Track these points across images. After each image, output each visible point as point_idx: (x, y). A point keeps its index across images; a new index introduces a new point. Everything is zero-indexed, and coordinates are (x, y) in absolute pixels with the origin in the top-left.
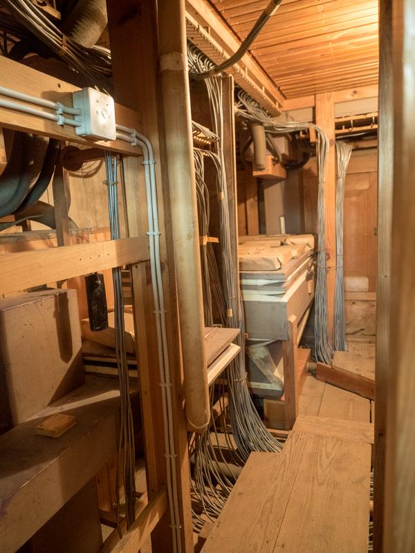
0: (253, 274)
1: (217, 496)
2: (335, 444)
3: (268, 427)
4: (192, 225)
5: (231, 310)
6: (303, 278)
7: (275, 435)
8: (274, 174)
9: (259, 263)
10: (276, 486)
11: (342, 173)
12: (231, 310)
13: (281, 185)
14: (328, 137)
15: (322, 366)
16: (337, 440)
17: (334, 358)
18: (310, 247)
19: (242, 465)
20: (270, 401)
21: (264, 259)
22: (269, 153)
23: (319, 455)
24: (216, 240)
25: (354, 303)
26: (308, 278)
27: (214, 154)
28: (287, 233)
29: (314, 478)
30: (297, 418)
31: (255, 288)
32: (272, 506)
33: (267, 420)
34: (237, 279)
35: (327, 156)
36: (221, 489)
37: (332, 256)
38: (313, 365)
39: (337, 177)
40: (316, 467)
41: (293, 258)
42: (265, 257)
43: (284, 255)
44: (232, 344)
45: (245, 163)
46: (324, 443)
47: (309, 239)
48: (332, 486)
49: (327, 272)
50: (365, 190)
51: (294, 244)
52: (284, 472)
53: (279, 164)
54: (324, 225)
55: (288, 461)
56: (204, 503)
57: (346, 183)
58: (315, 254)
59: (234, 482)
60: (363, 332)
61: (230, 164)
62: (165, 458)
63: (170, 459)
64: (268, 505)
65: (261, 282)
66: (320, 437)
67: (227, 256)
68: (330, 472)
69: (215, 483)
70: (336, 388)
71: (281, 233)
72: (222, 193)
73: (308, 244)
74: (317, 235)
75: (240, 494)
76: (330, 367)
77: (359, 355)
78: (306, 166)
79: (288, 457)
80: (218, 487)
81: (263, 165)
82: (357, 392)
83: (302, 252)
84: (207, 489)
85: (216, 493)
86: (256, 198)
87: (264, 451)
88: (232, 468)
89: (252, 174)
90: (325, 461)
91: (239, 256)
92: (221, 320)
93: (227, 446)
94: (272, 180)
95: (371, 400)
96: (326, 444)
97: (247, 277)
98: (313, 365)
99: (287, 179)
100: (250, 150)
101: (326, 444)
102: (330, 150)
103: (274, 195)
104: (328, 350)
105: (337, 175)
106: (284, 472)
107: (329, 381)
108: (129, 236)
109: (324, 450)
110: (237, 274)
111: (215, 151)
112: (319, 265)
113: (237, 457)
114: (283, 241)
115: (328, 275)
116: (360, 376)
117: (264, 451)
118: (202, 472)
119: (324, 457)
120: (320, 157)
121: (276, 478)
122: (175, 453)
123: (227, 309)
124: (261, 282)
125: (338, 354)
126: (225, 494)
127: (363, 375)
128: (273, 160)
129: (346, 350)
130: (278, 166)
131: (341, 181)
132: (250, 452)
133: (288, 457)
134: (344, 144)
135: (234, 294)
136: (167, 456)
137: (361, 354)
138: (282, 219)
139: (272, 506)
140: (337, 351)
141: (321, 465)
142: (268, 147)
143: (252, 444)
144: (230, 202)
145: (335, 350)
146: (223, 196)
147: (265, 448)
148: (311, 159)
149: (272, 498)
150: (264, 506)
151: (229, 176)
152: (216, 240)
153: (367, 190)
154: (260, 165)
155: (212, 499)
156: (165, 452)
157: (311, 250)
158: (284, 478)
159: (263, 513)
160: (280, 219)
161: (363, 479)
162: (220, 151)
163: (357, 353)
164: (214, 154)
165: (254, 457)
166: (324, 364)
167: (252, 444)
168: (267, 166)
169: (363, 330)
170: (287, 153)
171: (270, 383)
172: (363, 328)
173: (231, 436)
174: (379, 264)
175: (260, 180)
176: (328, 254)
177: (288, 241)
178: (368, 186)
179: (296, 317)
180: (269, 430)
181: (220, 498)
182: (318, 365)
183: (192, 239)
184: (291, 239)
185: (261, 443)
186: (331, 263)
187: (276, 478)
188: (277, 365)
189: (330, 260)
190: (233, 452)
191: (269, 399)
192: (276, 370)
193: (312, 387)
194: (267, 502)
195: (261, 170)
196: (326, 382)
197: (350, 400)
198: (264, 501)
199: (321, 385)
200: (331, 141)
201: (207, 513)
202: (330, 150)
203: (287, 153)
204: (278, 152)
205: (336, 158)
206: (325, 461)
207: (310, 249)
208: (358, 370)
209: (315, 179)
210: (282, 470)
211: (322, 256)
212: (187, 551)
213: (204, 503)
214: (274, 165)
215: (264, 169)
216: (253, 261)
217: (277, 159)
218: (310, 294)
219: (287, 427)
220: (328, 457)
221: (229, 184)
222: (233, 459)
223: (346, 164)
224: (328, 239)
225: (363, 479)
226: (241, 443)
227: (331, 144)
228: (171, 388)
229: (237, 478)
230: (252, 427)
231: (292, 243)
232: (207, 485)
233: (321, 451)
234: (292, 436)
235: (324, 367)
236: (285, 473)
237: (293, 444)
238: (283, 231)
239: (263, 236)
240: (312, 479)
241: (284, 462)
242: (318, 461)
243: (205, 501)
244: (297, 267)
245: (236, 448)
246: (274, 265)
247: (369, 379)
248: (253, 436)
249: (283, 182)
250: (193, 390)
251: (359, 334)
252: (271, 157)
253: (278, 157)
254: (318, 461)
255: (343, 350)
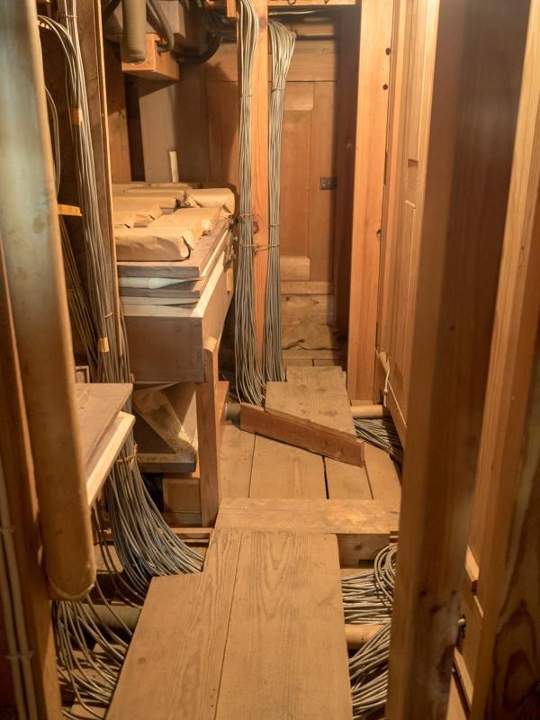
0: (139, 269)
1: (96, 666)
2: (286, 542)
3: (173, 524)
4: (43, 199)
5: (106, 340)
6: (220, 267)
7: (183, 536)
8: (160, 72)
9: (151, 248)
10: (201, 632)
11: (280, 82)
12: (106, 340)
13: (170, 90)
14: (257, 11)
15: (248, 408)
16: (287, 536)
17: (268, 393)
18: (227, 210)
19: (141, 603)
20: (174, 481)
21: (160, 240)
22: (150, 28)
23: (263, 565)
24: (75, 211)
25: (288, 299)
26: (226, 266)
27: (59, 25)
28: (181, 180)
29: (259, 608)
30: (221, 507)
31: (145, 292)
32: (197, 671)
33: (170, 511)
34: (113, 276)
35: (256, 47)
36: (103, 651)
37: (263, 226)
38: (236, 408)
39: (272, 91)
40: (261, 587)
41: (204, 234)
42: (161, 236)
43: (192, 231)
44: (121, 413)
45: (118, 47)
46: (269, 544)
47: (225, 197)
48: (289, 616)
49: (254, 253)
50: (306, 112)
51: (201, 206)
52: (210, 605)
53: (168, 53)
54: (249, 172)
55: (215, 587)
56: (76, 685)
57: (284, 99)
58: (236, 222)
59: (128, 639)
60: (303, 345)
61: (92, 50)
62: (9, 662)
63: (20, 662)
64: (192, 672)
65: (155, 282)
66: (259, 534)
67: (95, 239)
68: (282, 593)
69: (91, 642)
70: (272, 442)
71: (171, 181)
72: (80, 111)
73: (225, 207)
74: (241, 191)
75: (142, 660)
76: (262, 409)
77: (303, 386)
78: (212, 61)
79: (214, 576)
80: (98, 648)
81: (140, 53)
82: (305, 446)
83: (216, 222)
84: (77, 654)
85: (95, 661)
86: (124, 112)
87: (174, 573)
88: (119, 612)
89: (121, 67)
90: (273, 575)
91: (116, 233)
92: (86, 357)
93: (105, 568)
94: (155, 82)
95: (323, 457)
96: (271, 544)
97: (129, 273)
98: (236, 408)
99: (179, 83)
100: (115, 18)
101: (271, 544)
102: (260, 36)
103: (158, 110)
104: (257, 381)
105: (271, 82)
106: (210, 605)
107: (260, 432)
108: (54, 603)
109: (269, 555)
110: (112, 266)
111: (61, 20)
112: (241, 242)
113: (127, 587)
114: (181, 199)
115: (256, 259)
116: (309, 421)
117: (174, 573)
118: (68, 632)
119: (270, 569)
120: (245, 47)
121: (199, 620)
122: (30, 648)
123: (97, 338)
124: (155, 282)
125: (272, 387)
126: (112, 660)
127: (312, 421)
128: (158, 43)
129: (283, 379)
130: (166, 55)
131: (278, 95)
132: (149, 578)
133: (214, 576)
134: (283, 28)
135: (109, 309)
136: (14, 658)
137: (306, 384)
138: (173, 155)
139: (197, 671)
140: (270, 383)
141: (268, 584)
142: (150, 19)
143: (152, 565)
144: (97, 131)
145: (267, 380)
146: (81, 118)
147: (175, 569)
148: (222, 48)
149: (196, 657)
150: (185, 674)
151: (91, 77)
152: (75, 211)
153: (311, 112)
154: (134, 52)
155: (89, 674)
156: (6, 650)
157: (230, 217)
158: (213, 617)
159: (184, 686)
160: (169, 154)
161: (331, 596)
162: (72, 20)
163: (300, 382)
164: (59, 25)
165: (159, 587)
166: (252, 406)
167: (152, 565)
168: (150, 57)
169: (302, 341)
170: (183, 34)
171: (175, 453)
172: (300, 338)
173: (112, 549)
174: (502, 378)
175: (130, 79)
176: (255, 224)
177: (190, 200)
178: (312, 106)
179: (215, 341)
180: (175, 531)
181: (103, 668)
182: (242, 406)
183: (45, 231)
184: (196, 197)
185: (167, 560)
186: (261, 239)
187: (199, 620)
188: (182, 420)
189: (259, 235)
190: (116, 577)
191: (170, 478)
192: (182, 429)
193: (235, 444)
194: (188, 666)
195: (137, 61)
196: (256, 434)
197: (295, 460)
198: (184, 667)
199: (248, 438)
200: (261, 19)
201: (83, 700)
202: (260, 36)
203: (183, 34)
204: (169, 32)
205: (270, 53)
206: (273, 575)
207: (227, 214)
208: (304, 412)
209: (235, 92)
210: (208, 602)
211: (247, 226)
212: (32, 718)
213: (76, 685)
214: (159, 53)
215: (143, 60)
216: (138, 244)
217: (165, 42)
218: (229, 292)
219: (205, 520)
220: (276, 568)
221: (91, 93)
222: (118, 591)
223: (286, 64)
224: (257, 197)
225: (331, 596)
226: (131, 562)
227: (261, 26)
228: (14, 535)
229: (133, 631)
230: (150, 535)
231: (198, 204)
232: (76, 646)
233: (265, 557)
234: (216, 539)
235: (253, 410)
236: (213, 608)
237: (220, 554)
238: (175, 178)
239: (140, 184)
240: (256, 611)
241: (209, 587)
242: (263, 576)
243: (77, 681)
244: (214, 250)
245: (120, 569)
246: (178, 252)
247: (322, 426)
248: (153, 550)
249: (173, 86)
250: (60, 532)
251: (297, 347)
252: (154, 37)
253: (168, 40)
254: (263, 576)
255: (279, 379)
